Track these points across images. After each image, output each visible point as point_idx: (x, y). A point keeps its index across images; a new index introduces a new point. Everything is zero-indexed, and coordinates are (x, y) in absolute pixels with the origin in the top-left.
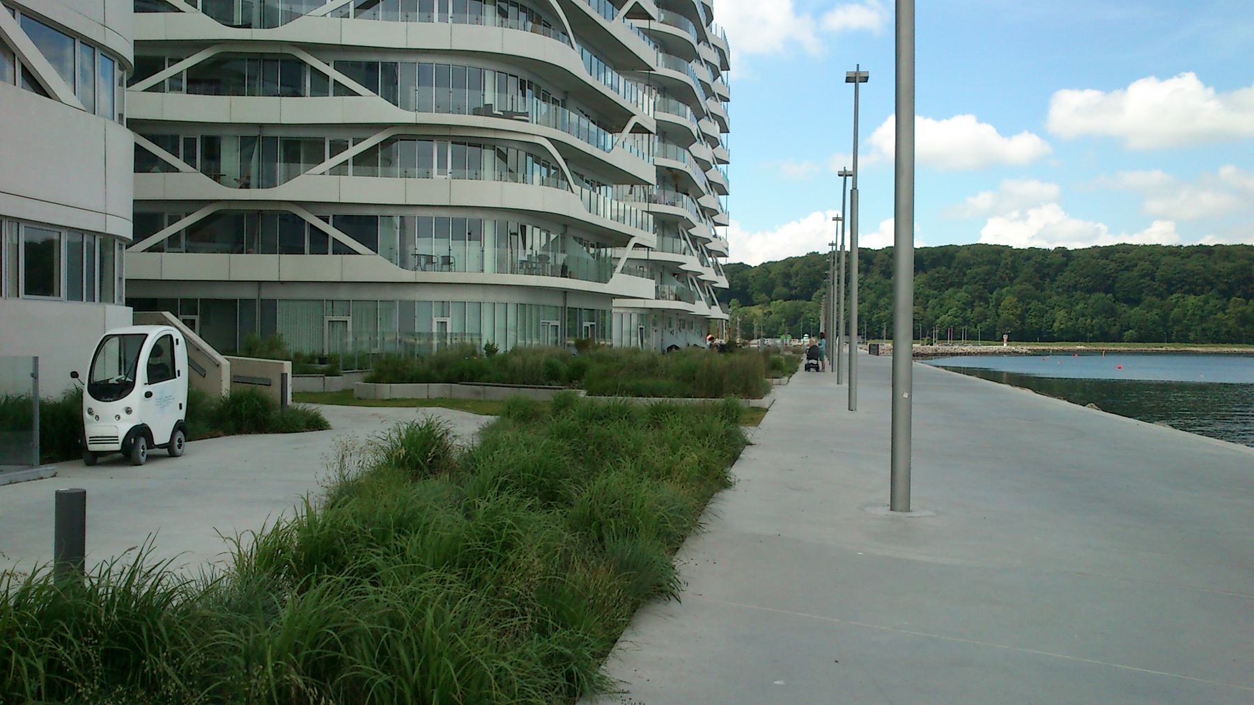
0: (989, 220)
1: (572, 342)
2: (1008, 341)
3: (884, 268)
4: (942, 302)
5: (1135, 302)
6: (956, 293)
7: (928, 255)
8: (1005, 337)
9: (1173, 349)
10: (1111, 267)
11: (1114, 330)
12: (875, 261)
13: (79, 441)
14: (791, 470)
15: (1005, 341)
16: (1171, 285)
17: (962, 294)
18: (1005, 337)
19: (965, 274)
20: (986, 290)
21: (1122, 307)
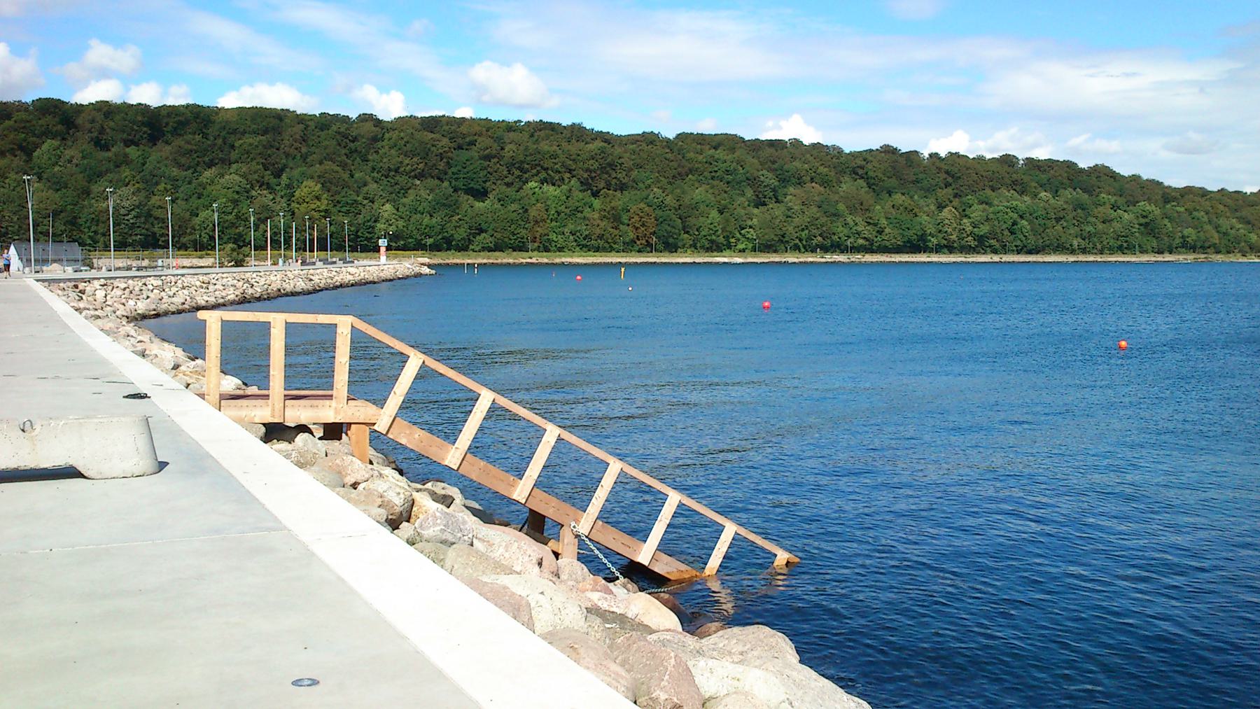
0: (807, 144)
1: (878, 207)
2: (389, 248)
3: (95, 134)
4: (200, 190)
5: (481, 194)
6: (222, 176)
7: (169, 115)
8: (383, 243)
9: (546, 261)
10: (441, 144)
11: (462, 233)
12: (79, 121)
13: (579, 278)
14: (245, 473)
15: (383, 250)
16: (524, 168)
17: (232, 178)
18: (383, 243)
19: (233, 147)
20: (269, 172)
21: (466, 200)
